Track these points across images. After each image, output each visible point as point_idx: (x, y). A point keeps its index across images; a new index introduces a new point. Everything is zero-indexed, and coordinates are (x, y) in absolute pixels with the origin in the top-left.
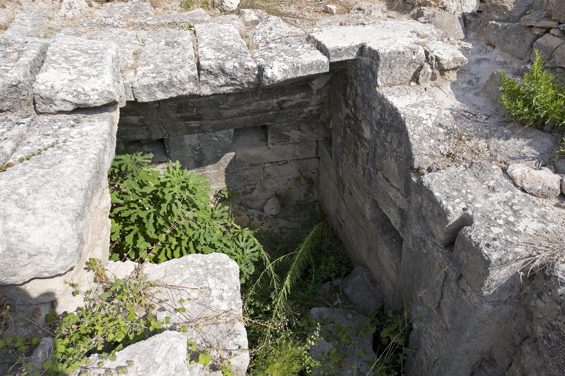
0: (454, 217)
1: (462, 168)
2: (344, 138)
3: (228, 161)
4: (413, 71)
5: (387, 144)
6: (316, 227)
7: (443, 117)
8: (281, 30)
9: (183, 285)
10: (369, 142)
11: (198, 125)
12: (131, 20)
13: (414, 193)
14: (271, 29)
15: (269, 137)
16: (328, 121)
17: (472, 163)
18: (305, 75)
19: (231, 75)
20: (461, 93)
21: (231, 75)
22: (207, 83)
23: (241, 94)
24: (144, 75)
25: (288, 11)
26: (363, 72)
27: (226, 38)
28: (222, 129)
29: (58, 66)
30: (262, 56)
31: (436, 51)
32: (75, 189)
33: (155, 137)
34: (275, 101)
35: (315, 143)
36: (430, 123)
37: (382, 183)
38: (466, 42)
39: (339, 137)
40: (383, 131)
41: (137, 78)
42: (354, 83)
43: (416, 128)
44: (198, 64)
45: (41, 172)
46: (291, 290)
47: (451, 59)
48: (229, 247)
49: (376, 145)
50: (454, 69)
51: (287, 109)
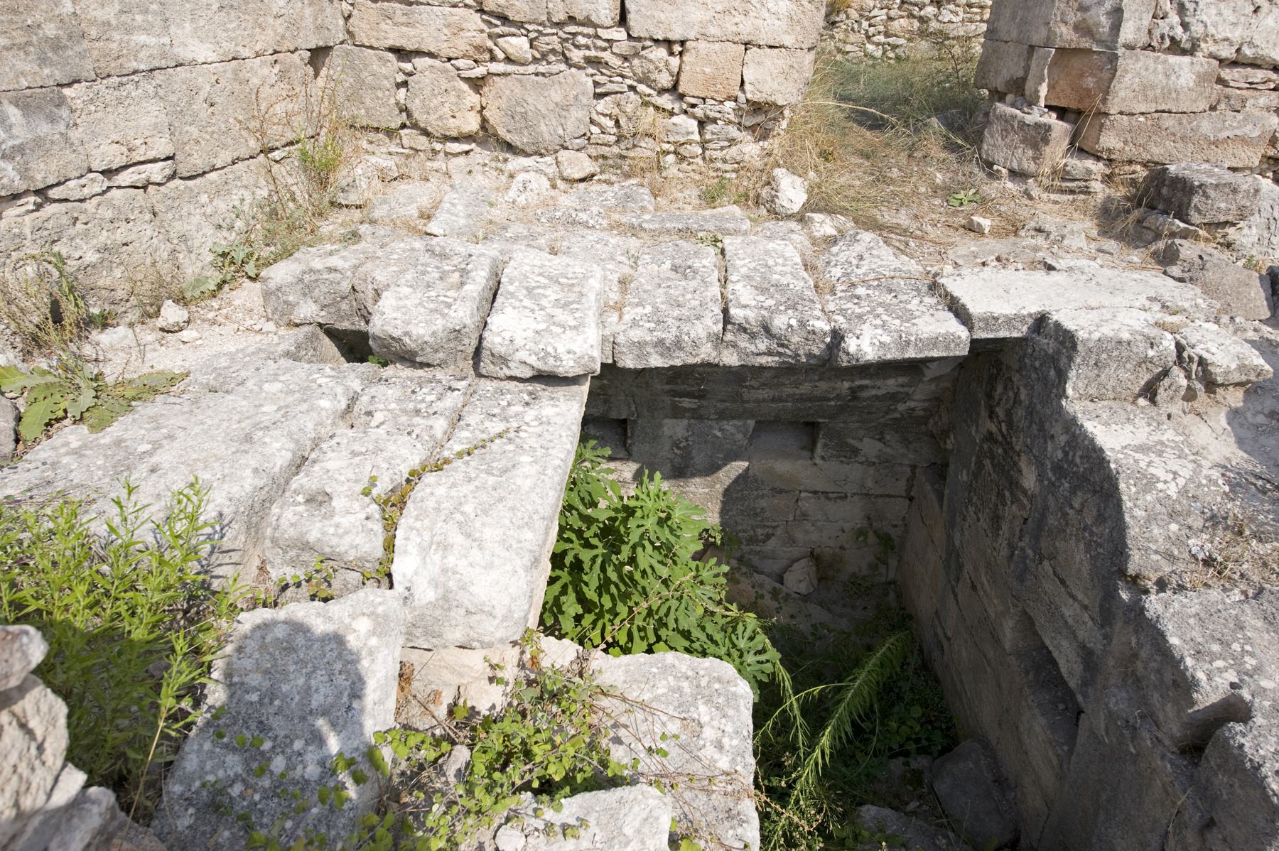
0: (1210, 691)
1: (1236, 596)
2: (976, 476)
3: (733, 475)
4: (1145, 377)
5: (1071, 512)
6: (892, 640)
7: (1204, 482)
8: (880, 263)
9: (654, 705)
10: (1032, 498)
11: (694, 406)
12: (616, 217)
13: (1120, 624)
14: (861, 258)
15: (819, 445)
16: (945, 433)
17: (1261, 590)
18: (919, 356)
19: (780, 339)
20: (1249, 435)
21: (780, 339)
22: (734, 346)
23: (788, 370)
24: (635, 324)
25: (895, 221)
26: (1037, 364)
27: (779, 269)
28: (733, 418)
29: (518, 304)
30: (842, 312)
31: (1202, 346)
32: (536, 517)
33: (614, 415)
34: (846, 385)
35: (908, 470)
36: (1172, 491)
37: (1050, 586)
38: (1273, 326)
39: (965, 472)
40: (1067, 485)
41: (623, 328)
42: (1014, 379)
43: (1140, 496)
44: (725, 311)
45: (491, 480)
46: (832, 755)
47: (1233, 366)
48: (716, 643)
49: (1046, 508)
50: (1237, 385)
51: (865, 400)
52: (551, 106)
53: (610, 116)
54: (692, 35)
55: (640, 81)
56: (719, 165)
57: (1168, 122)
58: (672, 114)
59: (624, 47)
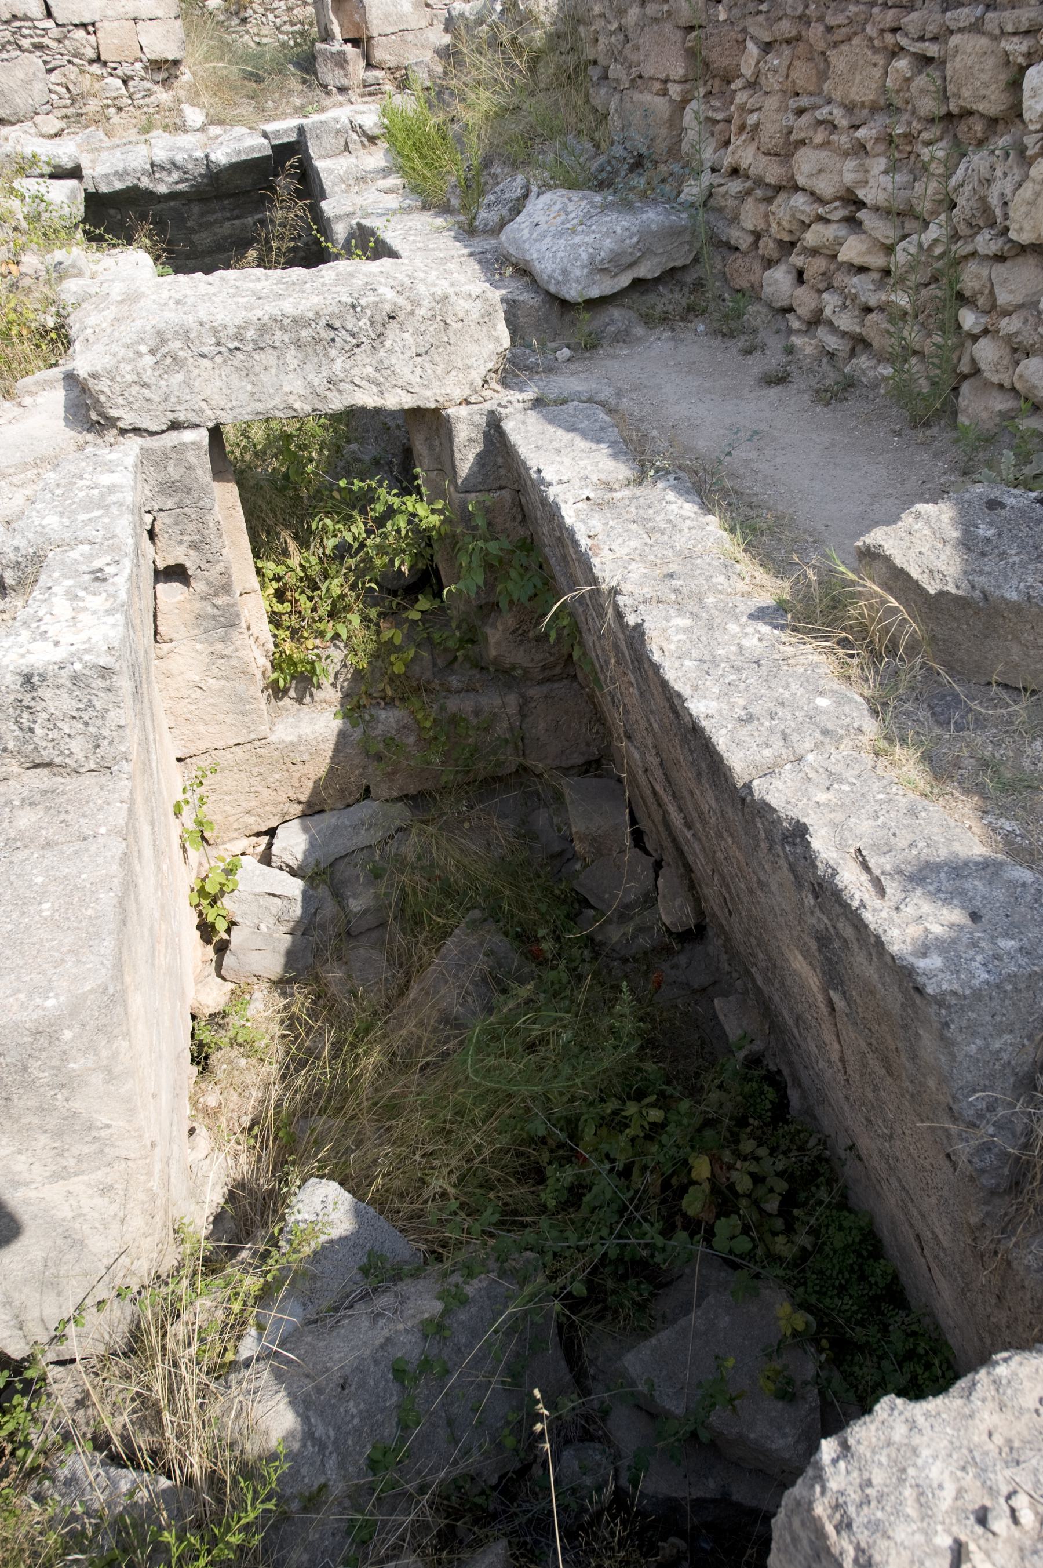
52: (19, 83)
53: (61, 84)
54: (97, 18)
55: (74, 56)
56: (145, 109)
57: (409, 37)
58: (103, 77)
59: (55, 32)
